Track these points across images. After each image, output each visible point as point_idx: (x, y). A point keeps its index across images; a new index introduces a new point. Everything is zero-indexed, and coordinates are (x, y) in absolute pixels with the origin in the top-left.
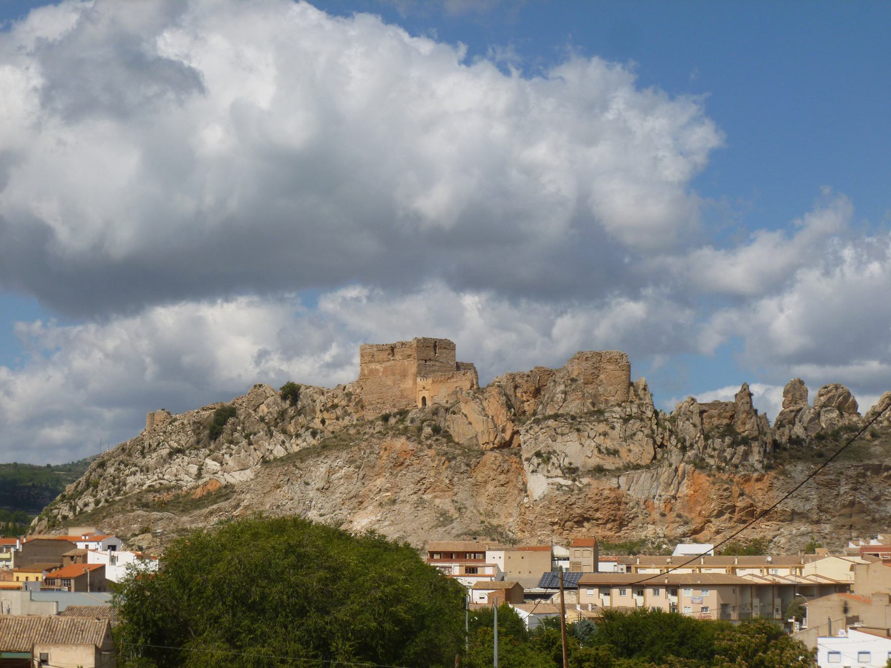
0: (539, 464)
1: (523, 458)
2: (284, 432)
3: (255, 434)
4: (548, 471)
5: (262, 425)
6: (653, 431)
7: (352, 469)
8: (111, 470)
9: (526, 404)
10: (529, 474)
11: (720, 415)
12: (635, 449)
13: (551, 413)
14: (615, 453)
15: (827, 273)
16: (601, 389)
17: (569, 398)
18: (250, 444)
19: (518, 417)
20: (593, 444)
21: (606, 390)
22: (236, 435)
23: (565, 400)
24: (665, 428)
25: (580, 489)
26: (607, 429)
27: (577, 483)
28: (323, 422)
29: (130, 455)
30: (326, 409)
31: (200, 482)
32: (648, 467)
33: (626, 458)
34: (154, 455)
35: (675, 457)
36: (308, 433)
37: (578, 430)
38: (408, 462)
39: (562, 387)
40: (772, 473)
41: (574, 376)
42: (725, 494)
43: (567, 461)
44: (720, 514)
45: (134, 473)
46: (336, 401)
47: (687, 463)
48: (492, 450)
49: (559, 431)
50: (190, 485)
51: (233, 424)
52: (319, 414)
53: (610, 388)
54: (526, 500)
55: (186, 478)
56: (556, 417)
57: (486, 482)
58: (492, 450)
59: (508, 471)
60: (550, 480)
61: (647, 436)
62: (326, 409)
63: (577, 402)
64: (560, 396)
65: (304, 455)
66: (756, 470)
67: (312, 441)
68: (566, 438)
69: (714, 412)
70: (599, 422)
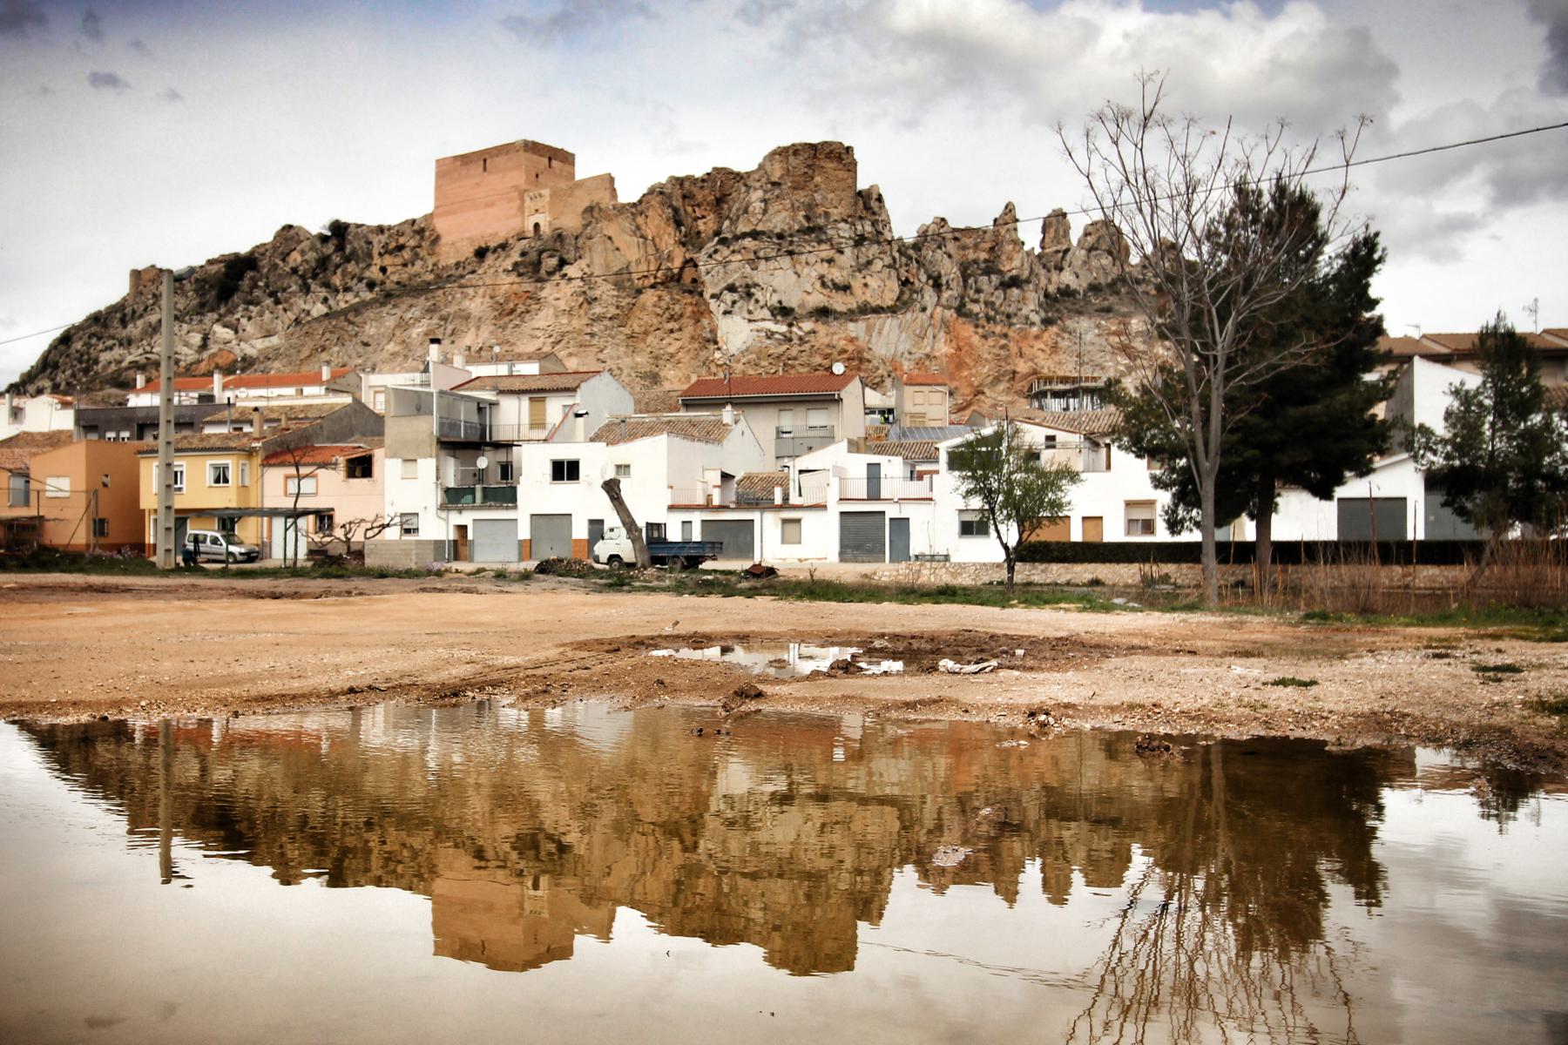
0: (734, 303)
1: (707, 296)
2: (327, 285)
3: (284, 290)
4: (750, 312)
5: (295, 278)
6: (894, 259)
7: (435, 321)
8: (78, 345)
9: (700, 222)
10: (720, 316)
11: (976, 246)
12: (873, 282)
13: (747, 230)
14: (846, 288)
15: (453, 498)
16: (818, 197)
17: (771, 211)
18: (277, 302)
19: (691, 240)
20: (814, 274)
21: (825, 198)
22: (257, 293)
23: (765, 211)
24: (910, 258)
25: (800, 338)
26: (832, 253)
27: (794, 329)
28: (383, 270)
29: (105, 326)
30: (386, 251)
31: (205, 355)
32: (893, 310)
33: (860, 296)
34: (140, 323)
35: (929, 296)
36: (362, 285)
37: (791, 253)
38: (521, 308)
39: (760, 193)
40: (1054, 329)
41: (775, 179)
42: (1002, 352)
43: (775, 298)
44: (997, 380)
45: (111, 348)
46: (402, 240)
47: (944, 307)
48: (653, 286)
49: (761, 254)
50: (190, 359)
51: (252, 279)
52: (377, 261)
53: (831, 195)
54: (717, 355)
55: (185, 350)
56: (755, 235)
57: (646, 333)
58: (653, 286)
59: (681, 316)
60: (753, 326)
61: (889, 266)
62: (386, 251)
63: (784, 214)
64: (757, 206)
65: (356, 310)
66: (1033, 324)
67: (368, 296)
68: (772, 264)
69: (969, 241)
70: (820, 242)
